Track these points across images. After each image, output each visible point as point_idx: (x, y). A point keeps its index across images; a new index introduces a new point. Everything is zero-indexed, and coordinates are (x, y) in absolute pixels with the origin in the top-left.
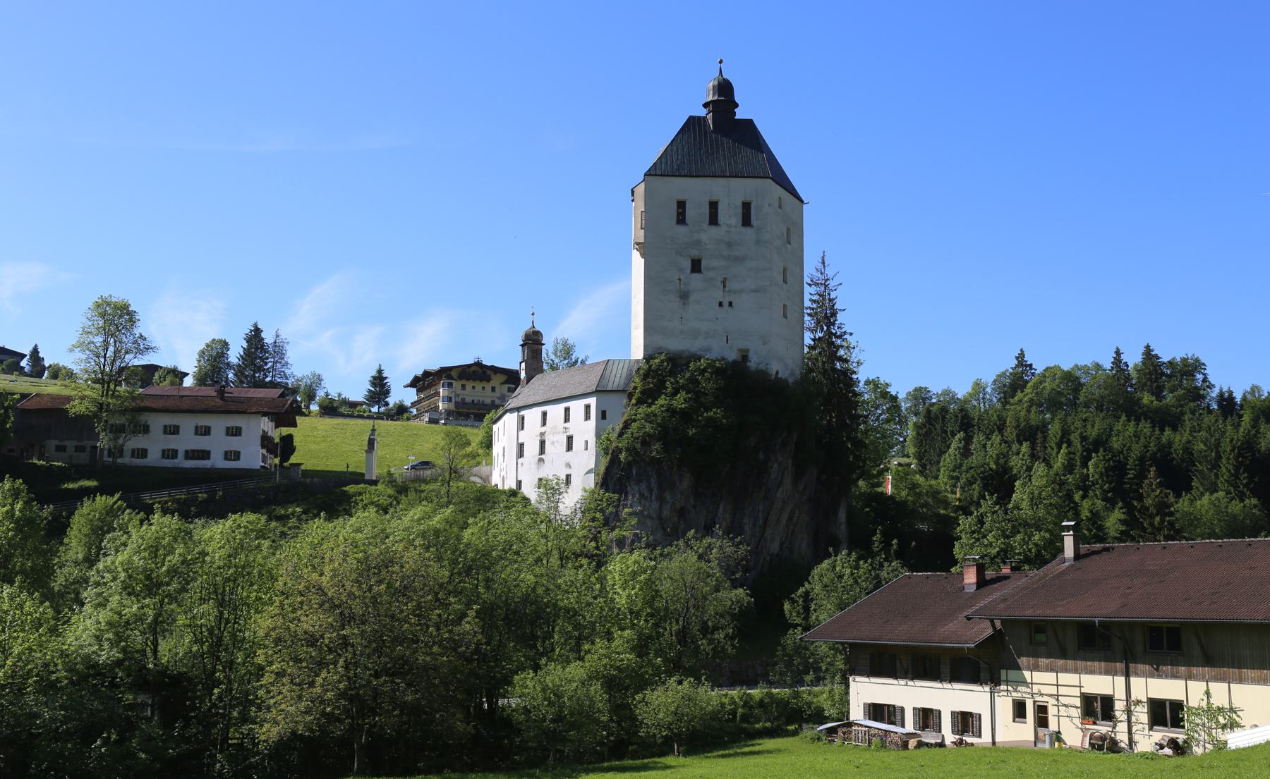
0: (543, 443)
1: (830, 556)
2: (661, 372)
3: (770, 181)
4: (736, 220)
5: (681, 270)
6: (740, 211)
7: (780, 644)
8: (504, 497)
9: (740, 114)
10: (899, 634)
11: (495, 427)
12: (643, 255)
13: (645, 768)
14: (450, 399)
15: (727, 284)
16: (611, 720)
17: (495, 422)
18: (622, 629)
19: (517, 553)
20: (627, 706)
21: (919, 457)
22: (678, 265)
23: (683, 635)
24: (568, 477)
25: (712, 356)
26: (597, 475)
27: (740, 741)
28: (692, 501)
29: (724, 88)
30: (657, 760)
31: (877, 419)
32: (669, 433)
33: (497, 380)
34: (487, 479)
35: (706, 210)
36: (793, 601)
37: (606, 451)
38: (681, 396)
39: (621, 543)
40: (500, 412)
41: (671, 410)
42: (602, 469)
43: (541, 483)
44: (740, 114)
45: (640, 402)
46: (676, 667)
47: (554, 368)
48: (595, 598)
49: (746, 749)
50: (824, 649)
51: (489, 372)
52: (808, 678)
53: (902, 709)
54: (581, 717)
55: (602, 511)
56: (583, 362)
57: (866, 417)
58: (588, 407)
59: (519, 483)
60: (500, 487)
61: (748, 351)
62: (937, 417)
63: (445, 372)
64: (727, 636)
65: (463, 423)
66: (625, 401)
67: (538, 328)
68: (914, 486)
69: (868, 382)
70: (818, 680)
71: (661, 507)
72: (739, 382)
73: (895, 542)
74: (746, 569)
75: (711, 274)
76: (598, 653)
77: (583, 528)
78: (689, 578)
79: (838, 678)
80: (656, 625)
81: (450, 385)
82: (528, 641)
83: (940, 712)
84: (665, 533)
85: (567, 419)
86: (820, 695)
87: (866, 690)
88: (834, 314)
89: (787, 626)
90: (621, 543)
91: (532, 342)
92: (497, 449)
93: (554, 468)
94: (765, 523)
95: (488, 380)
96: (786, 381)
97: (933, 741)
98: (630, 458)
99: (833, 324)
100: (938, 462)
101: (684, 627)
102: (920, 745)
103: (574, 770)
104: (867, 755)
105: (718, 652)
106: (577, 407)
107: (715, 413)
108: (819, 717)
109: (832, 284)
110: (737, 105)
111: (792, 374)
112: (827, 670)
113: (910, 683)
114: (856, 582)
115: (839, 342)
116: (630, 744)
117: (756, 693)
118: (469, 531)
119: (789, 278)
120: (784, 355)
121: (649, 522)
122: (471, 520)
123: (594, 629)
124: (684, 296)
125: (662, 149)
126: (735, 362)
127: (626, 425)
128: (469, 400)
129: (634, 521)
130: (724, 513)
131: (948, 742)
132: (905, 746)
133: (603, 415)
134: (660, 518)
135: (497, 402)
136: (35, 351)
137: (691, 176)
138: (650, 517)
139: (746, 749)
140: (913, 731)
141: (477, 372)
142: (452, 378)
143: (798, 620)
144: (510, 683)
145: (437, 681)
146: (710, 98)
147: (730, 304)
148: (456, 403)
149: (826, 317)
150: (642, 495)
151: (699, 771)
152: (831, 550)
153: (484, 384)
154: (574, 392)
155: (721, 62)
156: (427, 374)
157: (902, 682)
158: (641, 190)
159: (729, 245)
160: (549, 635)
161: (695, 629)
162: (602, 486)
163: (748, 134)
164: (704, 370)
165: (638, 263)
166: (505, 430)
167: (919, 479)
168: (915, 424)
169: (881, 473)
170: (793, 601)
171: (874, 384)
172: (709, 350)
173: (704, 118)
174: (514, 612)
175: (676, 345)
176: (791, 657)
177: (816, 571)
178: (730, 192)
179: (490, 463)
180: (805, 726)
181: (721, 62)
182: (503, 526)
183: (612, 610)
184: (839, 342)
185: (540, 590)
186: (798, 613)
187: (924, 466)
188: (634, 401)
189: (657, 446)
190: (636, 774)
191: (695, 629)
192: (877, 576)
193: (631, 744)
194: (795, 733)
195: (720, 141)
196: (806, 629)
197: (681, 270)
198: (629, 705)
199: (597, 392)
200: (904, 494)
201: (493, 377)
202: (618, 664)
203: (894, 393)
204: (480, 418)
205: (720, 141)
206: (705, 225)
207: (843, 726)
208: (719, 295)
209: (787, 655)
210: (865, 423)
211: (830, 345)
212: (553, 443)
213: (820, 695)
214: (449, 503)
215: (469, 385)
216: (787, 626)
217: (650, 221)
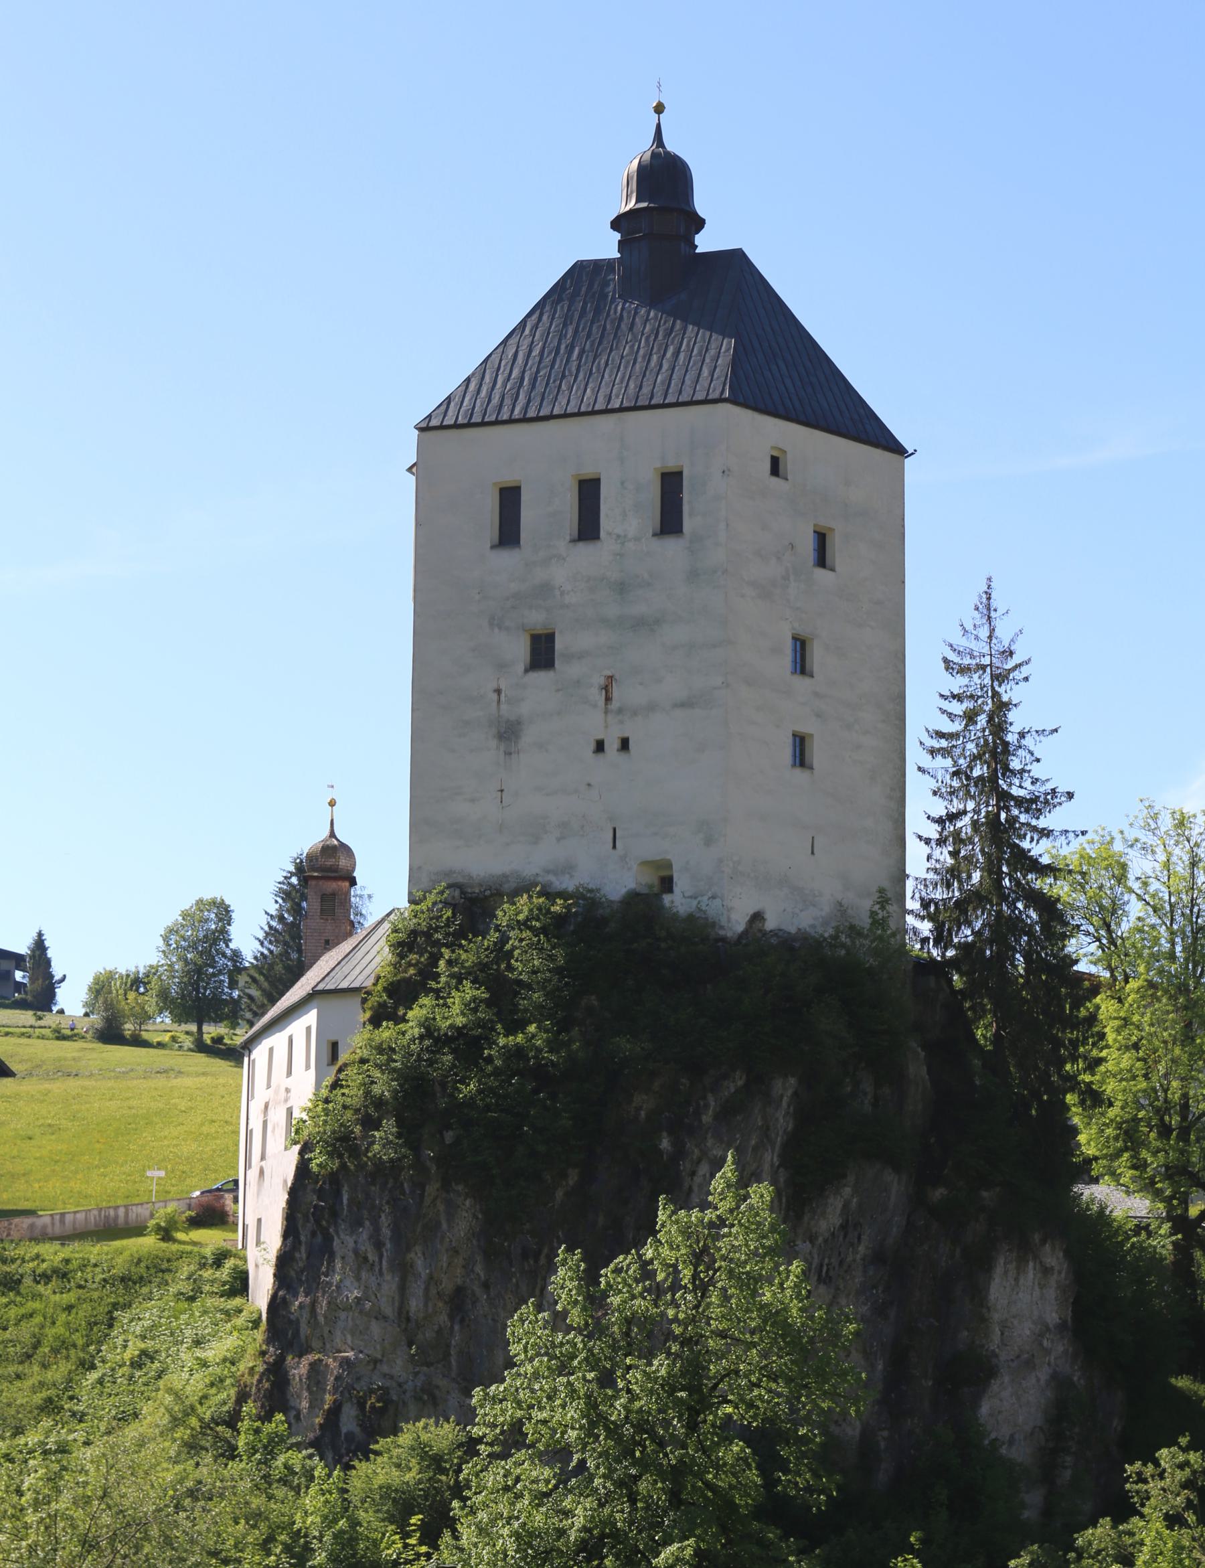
5: (502, 666)
15: (616, 693)
28: (479, 1269)
35: (568, 504)
61: (668, 865)
67: (343, 836)
71: (403, 1288)
110: (699, 223)
121: (376, 1328)
124: (508, 733)
125: (469, 366)
126: (633, 898)
136: (40, 945)
138: (380, 1316)
147: (625, 744)
155: (659, 109)
159: (622, 588)
172: (568, 868)
175: (482, 863)
197: (502, 666)
206: (562, 545)
208: (594, 724)
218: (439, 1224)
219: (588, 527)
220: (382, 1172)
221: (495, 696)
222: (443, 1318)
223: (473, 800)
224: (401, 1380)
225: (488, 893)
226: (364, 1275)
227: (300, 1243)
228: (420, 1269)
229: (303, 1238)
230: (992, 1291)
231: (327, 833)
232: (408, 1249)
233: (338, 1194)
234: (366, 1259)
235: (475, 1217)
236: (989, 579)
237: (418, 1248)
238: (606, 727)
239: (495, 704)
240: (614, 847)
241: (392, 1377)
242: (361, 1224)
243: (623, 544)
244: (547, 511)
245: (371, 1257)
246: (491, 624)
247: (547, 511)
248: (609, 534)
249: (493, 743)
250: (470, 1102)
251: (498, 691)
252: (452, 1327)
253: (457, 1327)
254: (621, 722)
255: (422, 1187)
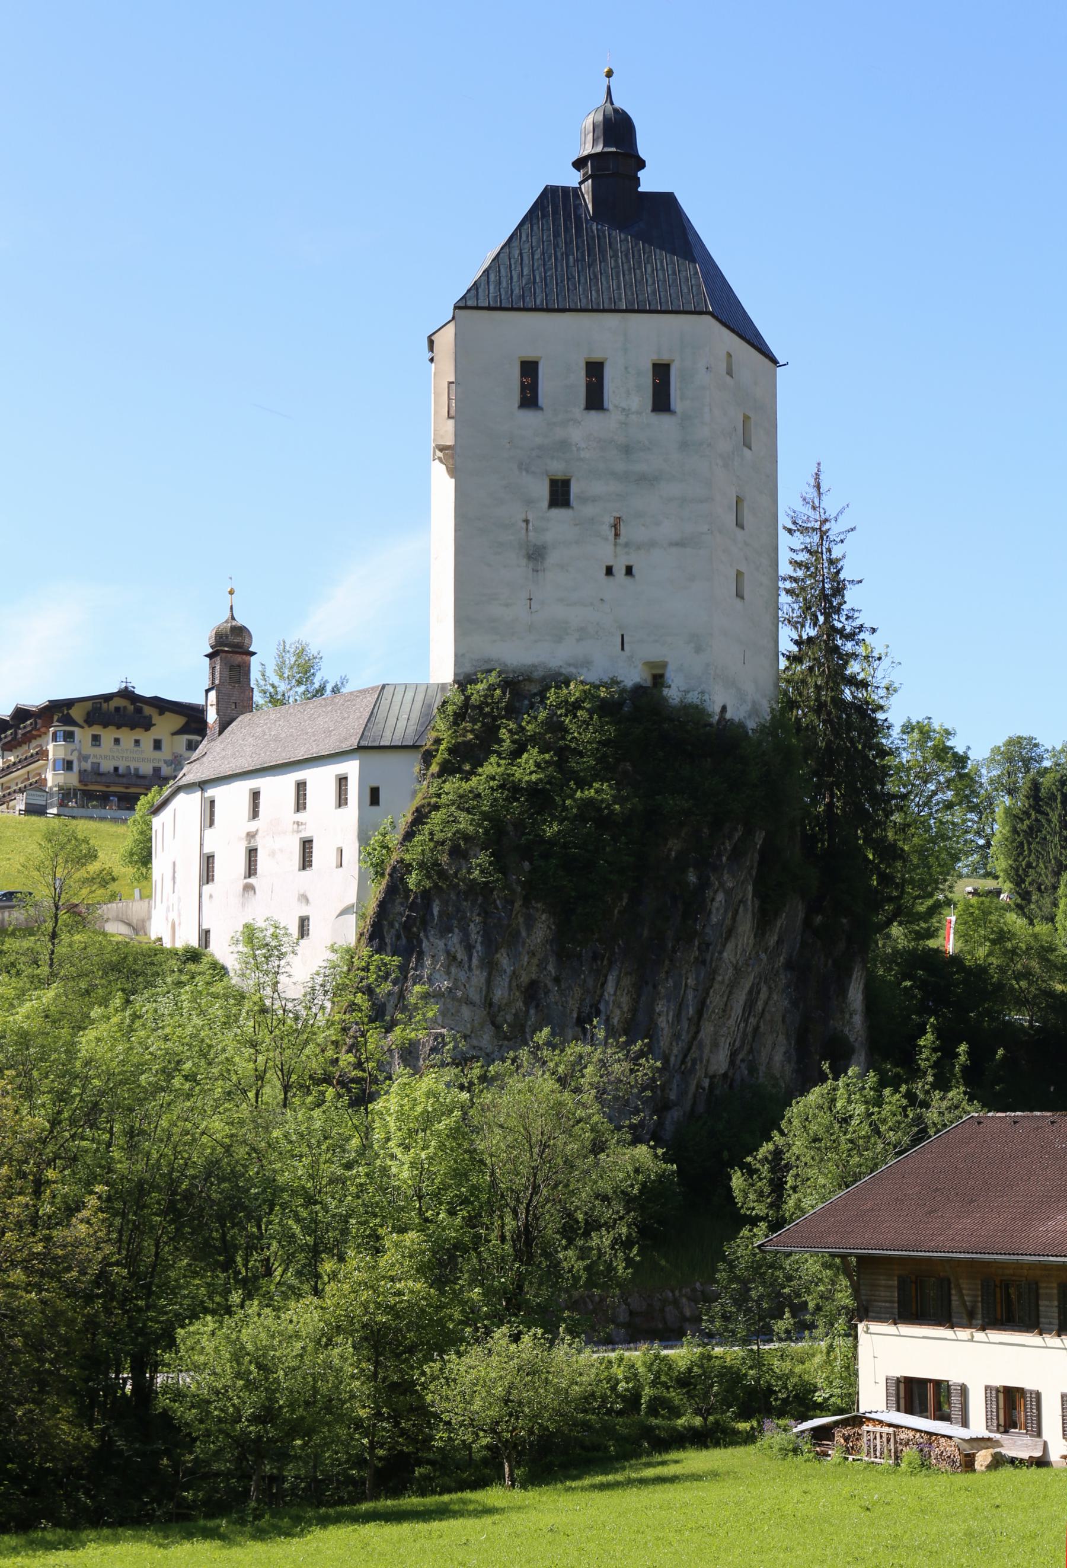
0: (252, 853)
1: (823, 1079)
2: (488, 711)
3: (708, 318)
4: (642, 399)
5: (529, 502)
6: (648, 380)
7: (724, 1259)
8: (174, 963)
9: (649, 182)
10: (953, 1235)
11: (157, 822)
12: (452, 472)
13: (442, 1513)
14: (68, 765)
15: (623, 530)
16: (378, 1415)
17: (157, 810)
18: (402, 1231)
19: (189, 1077)
20: (406, 1387)
21: (1018, 878)
22: (521, 489)
23: (526, 1239)
24: (304, 924)
25: (592, 676)
26: (363, 917)
27: (639, 1456)
28: (551, 968)
29: (617, 129)
30: (468, 1495)
31: (927, 804)
32: (505, 832)
33: (164, 726)
34: (139, 928)
35: (579, 379)
36: (750, 1171)
37: (379, 869)
38: (531, 757)
39: (409, 1054)
40: (167, 791)
41: (510, 788)
42: (372, 906)
43: (250, 934)
44: (649, 182)
45: (447, 770)
46: (512, 1307)
47: (276, 700)
48: (348, 1166)
49: (650, 1472)
50: (811, 1266)
51: (148, 710)
52: (780, 1326)
53: (964, 1390)
54: (323, 1407)
55: (369, 991)
56: (336, 690)
57: (904, 797)
58: (342, 781)
59: (205, 936)
60: (167, 944)
61: (664, 665)
62: (1052, 797)
63: (58, 712)
64: (615, 1241)
65: (96, 813)
66: (417, 767)
67: (241, 621)
68: (1001, 937)
69: (908, 728)
70: (803, 1328)
71: (489, 981)
72: (647, 727)
73: (963, 1048)
74: (662, 1107)
75: (589, 510)
76: (353, 1283)
77: (330, 1024)
78: (537, 1126)
79: (840, 1325)
80: (471, 1222)
81: (69, 737)
82: (218, 1255)
83: (1038, 1395)
84: (498, 1032)
85: (300, 804)
86: (802, 1358)
87: (891, 1351)
88: (839, 590)
89: (739, 1220)
90: (409, 1054)
91: (231, 649)
92: (160, 865)
93: (276, 902)
94: (700, 1013)
95: (147, 725)
96: (741, 725)
97: (1025, 1455)
98: (428, 884)
99: (838, 611)
100: (1055, 888)
101: (527, 1225)
102: (999, 1462)
103: (297, 1520)
104: (891, 1482)
105: (598, 1273)
106: (320, 780)
107: (600, 791)
108: (802, 1403)
109: (834, 529)
110: (641, 164)
111: (754, 711)
112: (818, 1308)
113: (979, 1335)
114: (877, 1132)
115: (849, 647)
116: (410, 1466)
117: (681, 1355)
118: (91, 1034)
119: (748, 518)
120: (734, 678)
121: (466, 1012)
122: (96, 1012)
123: (345, 1232)
124: (536, 555)
126: (638, 689)
127: (420, 817)
128: (107, 766)
129: (432, 1011)
130: (616, 992)
131: (1054, 1456)
132: (968, 1464)
133: (374, 796)
134: (489, 1003)
135: (166, 771)
137: (548, 310)
138: (469, 1002)
139: (650, 1472)
140: (986, 1434)
141: (124, 711)
142: (74, 723)
143: (760, 1209)
144: (171, 1344)
145: (18, 1342)
146: (588, 150)
147: (629, 571)
148: (82, 773)
149: (824, 597)
150: (452, 958)
151: (548, 1520)
152: (826, 1066)
153: (138, 734)
154: (314, 752)
155: (609, 74)
156: (21, 714)
157: (963, 1334)
158: (446, 339)
159: (627, 450)
160: (254, 1244)
161: (550, 1225)
162: (371, 938)
163: (663, 224)
164: (577, 706)
165: (442, 487)
166: (174, 825)
167: (1014, 920)
168: (1008, 811)
169: (936, 909)
170: (751, 1171)
171: (922, 731)
172: (587, 663)
173: (576, 191)
174: (188, 1196)
176: (745, 1283)
177: (796, 1109)
178: (629, 343)
179: (147, 896)
180: (768, 1424)
181: (609, 74)
182: (169, 1018)
183: (383, 1189)
184: (849, 647)
185: (241, 1152)
186: (761, 1194)
187: (1026, 896)
188: (434, 768)
189: (482, 858)
190: (421, 1527)
191: (550, 1225)
192: (919, 1119)
193: (419, 1463)
194: (749, 1439)
195: (609, 234)
196: (776, 1225)
197: (529, 502)
198: (413, 1383)
199: (361, 749)
200: (981, 952)
201: (156, 719)
202: (392, 1300)
203: (960, 750)
204: (128, 802)
205: (609, 234)
207: (844, 1423)
208: (606, 552)
209: (736, 1279)
210: (900, 809)
211: (830, 651)
212: (273, 854)
213: (802, 1358)
214: (53, 975)
215: (108, 735)
216: (739, 1220)
217: (464, 404)
218: (518, 932)
219: (595, 400)
220: (480, 892)
221: (524, 525)
222: (520, 1004)
223: (507, 605)
224: (488, 1051)
225: (521, 678)
226: (453, 970)
227: (386, 944)
228: (505, 967)
229: (388, 940)
230: (850, 994)
231: (228, 615)
232: (496, 952)
233: (428, 907)
234: (455, 958)
235: (549, 927)
236: (819, 464)
237: (503, 951)
238: (616, 556)
239: (524, 531)
240: (623, 649)
241: (481, 1049)
242: (451, 931)
243: (627, 415)
244: (561, 383)
245: (459, 957)
246: (520, 468)
247: (561, 383)
248: (616, 407)
249: (524, 562)
250: (552, 842)
251: (527, 521)
252: (527, 1012)
253: (532, 1012)
254: (627, 553)
255: (512, 903)
